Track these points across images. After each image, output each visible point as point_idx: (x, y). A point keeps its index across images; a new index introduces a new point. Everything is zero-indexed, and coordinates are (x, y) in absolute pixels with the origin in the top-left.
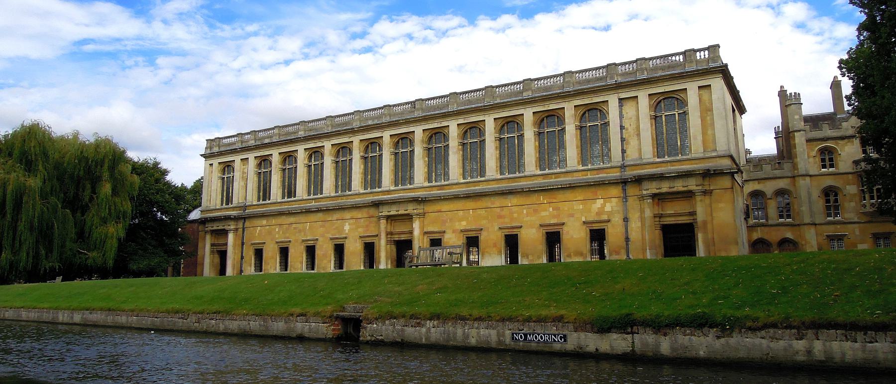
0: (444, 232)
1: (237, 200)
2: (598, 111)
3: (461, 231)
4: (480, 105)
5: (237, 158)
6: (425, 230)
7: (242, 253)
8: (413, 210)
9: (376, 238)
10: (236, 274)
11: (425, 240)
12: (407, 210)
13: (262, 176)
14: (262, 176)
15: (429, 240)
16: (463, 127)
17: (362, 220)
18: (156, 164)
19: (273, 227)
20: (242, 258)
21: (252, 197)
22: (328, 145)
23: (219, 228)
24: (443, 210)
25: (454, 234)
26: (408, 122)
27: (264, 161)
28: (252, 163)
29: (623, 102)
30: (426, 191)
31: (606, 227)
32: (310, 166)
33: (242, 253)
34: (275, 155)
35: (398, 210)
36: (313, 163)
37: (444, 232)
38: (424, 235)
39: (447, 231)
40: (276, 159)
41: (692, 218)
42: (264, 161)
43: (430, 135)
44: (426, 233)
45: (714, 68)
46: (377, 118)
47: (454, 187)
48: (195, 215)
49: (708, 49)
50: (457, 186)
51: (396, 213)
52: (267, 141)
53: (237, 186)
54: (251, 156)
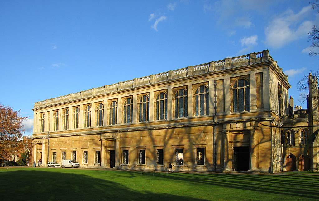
1: (46, 130)
2: (244, 80)
5: (46, 111)
7: (48, 154)
10: (293, 129)
13: (142, 106)
14: (142, 106)
18: (295, 70)
19: (60, 142)
20: (48, 156)
21: (52, 130)
22: (81, 104)
26: (102, 96)
27: (57, 111)
28: (52, 113)
29: (217, 82)
32: (158, 102)
33: (48, 154)
34: (61, 109)
36: (160, 100)
40: (61, 111)
42: (57, 111)
48: (18, 141)
49: (167, 73)
52: (57, 103)
53: (46, 123)
54: (51, 109)
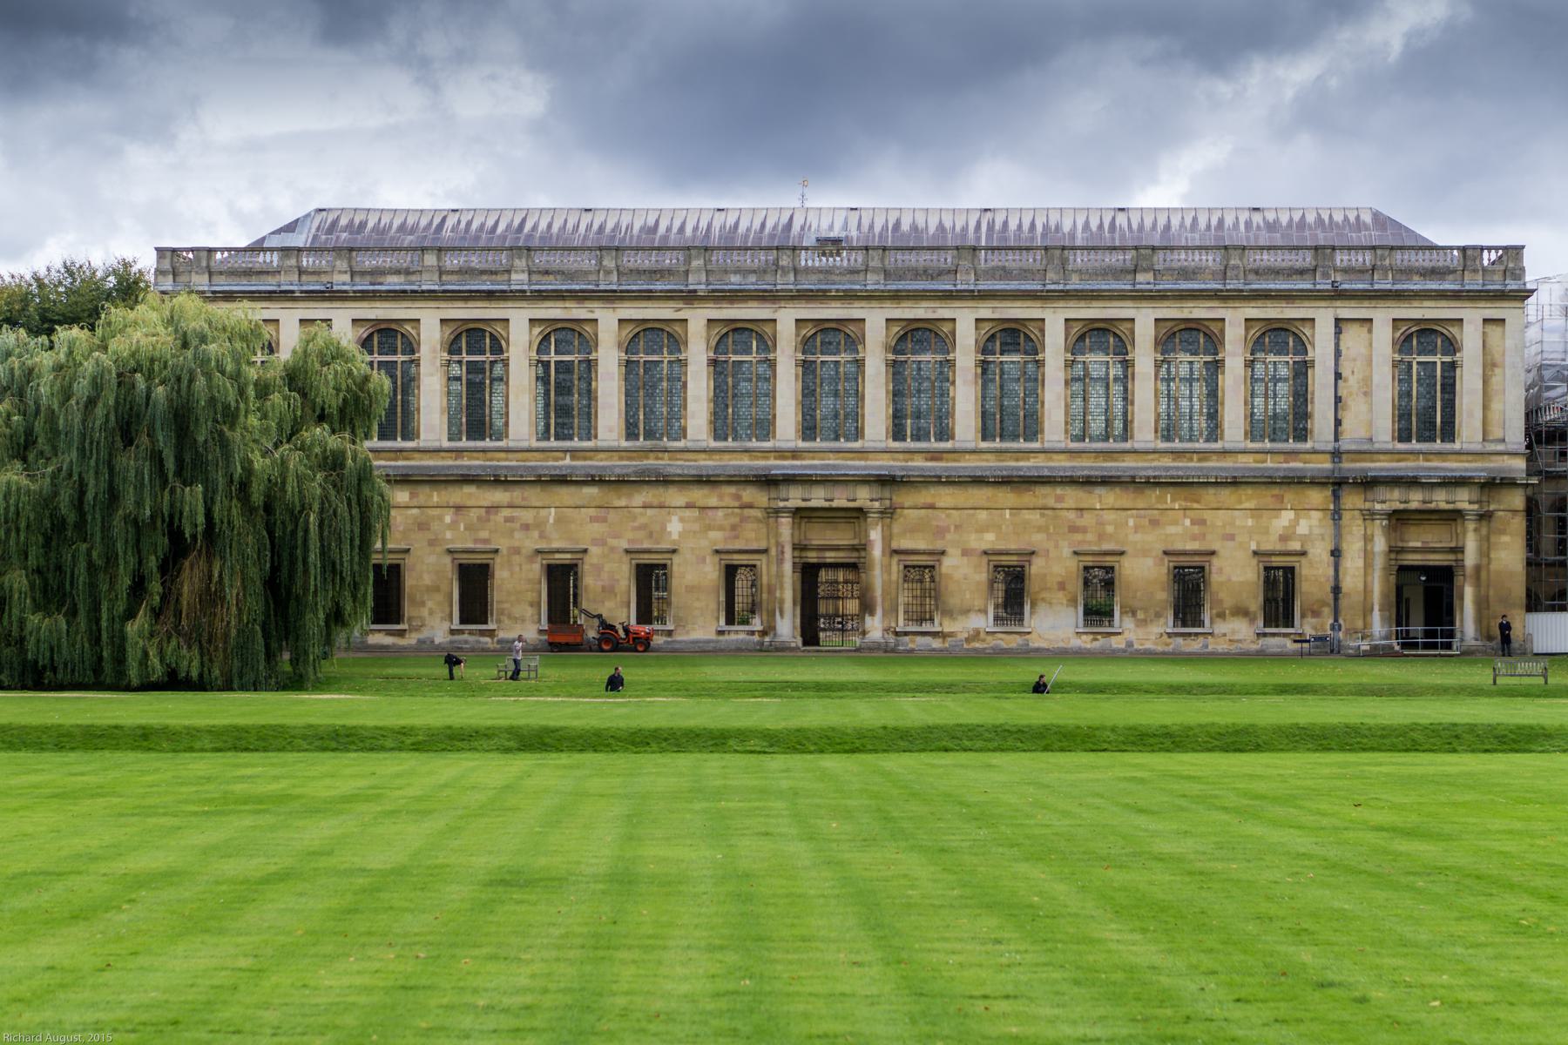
0: (943, 553)
3: (985, 553)
4: (858, 287)
6: (895, 545)
8: (872, 500)
9: (763, 557)
11: (894, 568)
12: (854, 500)
15: (901, 567)
16: (987, 326)
17: (720, 513)
23: (835, 504)
24: (939, 504)
25: (965, 558)
30: (894, 460)
31: (758, 563)
35: (829, 497)
37: (943, 553)
38: (891, 556)
39: (950, 550)
41: (855, 554)
43: (902, 333)
44: (896, 552)
45: (782, 290)
46: (754, 272)
47: (967, 456)
50: (973, 457)
51: (827, 504)
